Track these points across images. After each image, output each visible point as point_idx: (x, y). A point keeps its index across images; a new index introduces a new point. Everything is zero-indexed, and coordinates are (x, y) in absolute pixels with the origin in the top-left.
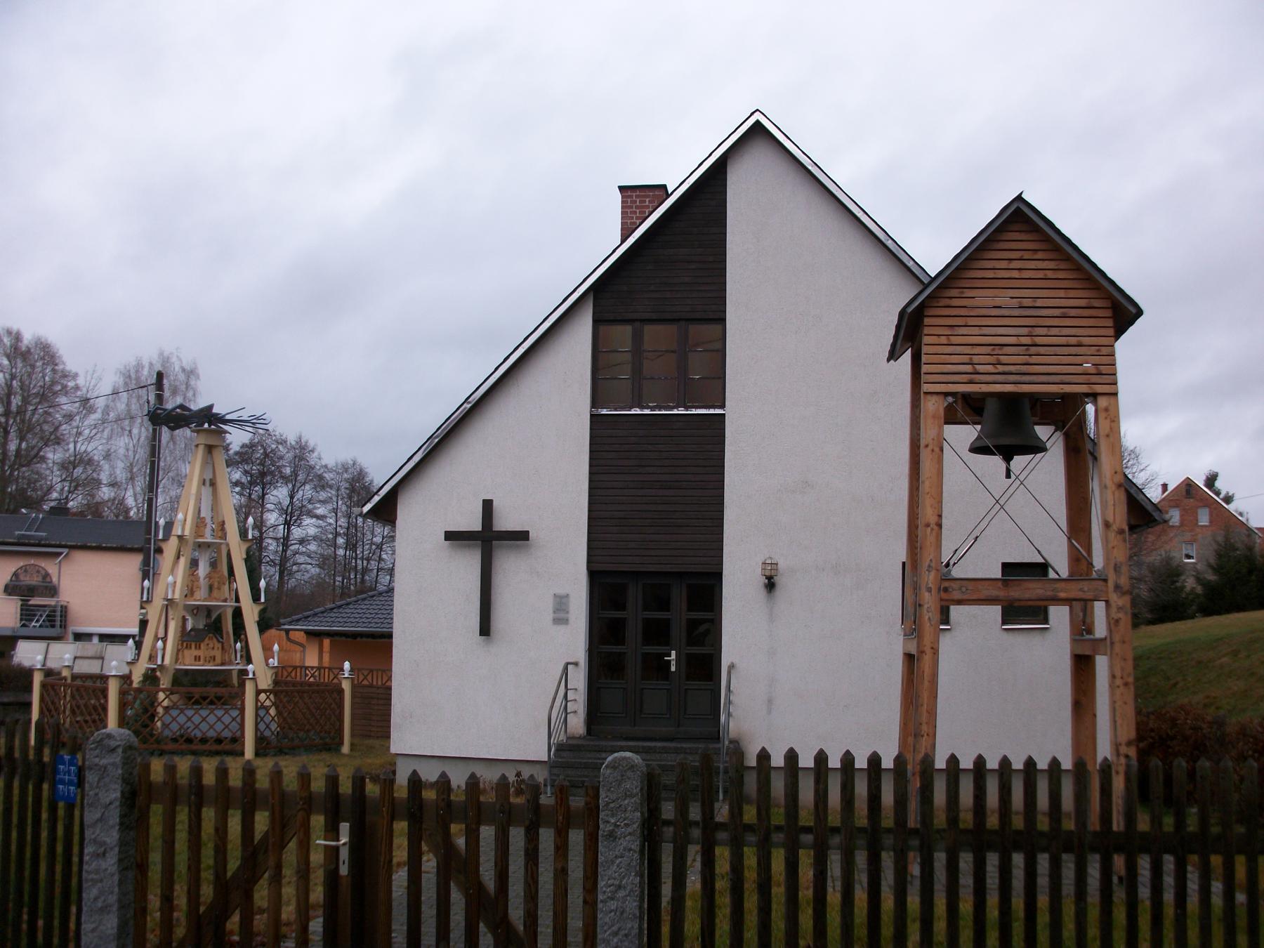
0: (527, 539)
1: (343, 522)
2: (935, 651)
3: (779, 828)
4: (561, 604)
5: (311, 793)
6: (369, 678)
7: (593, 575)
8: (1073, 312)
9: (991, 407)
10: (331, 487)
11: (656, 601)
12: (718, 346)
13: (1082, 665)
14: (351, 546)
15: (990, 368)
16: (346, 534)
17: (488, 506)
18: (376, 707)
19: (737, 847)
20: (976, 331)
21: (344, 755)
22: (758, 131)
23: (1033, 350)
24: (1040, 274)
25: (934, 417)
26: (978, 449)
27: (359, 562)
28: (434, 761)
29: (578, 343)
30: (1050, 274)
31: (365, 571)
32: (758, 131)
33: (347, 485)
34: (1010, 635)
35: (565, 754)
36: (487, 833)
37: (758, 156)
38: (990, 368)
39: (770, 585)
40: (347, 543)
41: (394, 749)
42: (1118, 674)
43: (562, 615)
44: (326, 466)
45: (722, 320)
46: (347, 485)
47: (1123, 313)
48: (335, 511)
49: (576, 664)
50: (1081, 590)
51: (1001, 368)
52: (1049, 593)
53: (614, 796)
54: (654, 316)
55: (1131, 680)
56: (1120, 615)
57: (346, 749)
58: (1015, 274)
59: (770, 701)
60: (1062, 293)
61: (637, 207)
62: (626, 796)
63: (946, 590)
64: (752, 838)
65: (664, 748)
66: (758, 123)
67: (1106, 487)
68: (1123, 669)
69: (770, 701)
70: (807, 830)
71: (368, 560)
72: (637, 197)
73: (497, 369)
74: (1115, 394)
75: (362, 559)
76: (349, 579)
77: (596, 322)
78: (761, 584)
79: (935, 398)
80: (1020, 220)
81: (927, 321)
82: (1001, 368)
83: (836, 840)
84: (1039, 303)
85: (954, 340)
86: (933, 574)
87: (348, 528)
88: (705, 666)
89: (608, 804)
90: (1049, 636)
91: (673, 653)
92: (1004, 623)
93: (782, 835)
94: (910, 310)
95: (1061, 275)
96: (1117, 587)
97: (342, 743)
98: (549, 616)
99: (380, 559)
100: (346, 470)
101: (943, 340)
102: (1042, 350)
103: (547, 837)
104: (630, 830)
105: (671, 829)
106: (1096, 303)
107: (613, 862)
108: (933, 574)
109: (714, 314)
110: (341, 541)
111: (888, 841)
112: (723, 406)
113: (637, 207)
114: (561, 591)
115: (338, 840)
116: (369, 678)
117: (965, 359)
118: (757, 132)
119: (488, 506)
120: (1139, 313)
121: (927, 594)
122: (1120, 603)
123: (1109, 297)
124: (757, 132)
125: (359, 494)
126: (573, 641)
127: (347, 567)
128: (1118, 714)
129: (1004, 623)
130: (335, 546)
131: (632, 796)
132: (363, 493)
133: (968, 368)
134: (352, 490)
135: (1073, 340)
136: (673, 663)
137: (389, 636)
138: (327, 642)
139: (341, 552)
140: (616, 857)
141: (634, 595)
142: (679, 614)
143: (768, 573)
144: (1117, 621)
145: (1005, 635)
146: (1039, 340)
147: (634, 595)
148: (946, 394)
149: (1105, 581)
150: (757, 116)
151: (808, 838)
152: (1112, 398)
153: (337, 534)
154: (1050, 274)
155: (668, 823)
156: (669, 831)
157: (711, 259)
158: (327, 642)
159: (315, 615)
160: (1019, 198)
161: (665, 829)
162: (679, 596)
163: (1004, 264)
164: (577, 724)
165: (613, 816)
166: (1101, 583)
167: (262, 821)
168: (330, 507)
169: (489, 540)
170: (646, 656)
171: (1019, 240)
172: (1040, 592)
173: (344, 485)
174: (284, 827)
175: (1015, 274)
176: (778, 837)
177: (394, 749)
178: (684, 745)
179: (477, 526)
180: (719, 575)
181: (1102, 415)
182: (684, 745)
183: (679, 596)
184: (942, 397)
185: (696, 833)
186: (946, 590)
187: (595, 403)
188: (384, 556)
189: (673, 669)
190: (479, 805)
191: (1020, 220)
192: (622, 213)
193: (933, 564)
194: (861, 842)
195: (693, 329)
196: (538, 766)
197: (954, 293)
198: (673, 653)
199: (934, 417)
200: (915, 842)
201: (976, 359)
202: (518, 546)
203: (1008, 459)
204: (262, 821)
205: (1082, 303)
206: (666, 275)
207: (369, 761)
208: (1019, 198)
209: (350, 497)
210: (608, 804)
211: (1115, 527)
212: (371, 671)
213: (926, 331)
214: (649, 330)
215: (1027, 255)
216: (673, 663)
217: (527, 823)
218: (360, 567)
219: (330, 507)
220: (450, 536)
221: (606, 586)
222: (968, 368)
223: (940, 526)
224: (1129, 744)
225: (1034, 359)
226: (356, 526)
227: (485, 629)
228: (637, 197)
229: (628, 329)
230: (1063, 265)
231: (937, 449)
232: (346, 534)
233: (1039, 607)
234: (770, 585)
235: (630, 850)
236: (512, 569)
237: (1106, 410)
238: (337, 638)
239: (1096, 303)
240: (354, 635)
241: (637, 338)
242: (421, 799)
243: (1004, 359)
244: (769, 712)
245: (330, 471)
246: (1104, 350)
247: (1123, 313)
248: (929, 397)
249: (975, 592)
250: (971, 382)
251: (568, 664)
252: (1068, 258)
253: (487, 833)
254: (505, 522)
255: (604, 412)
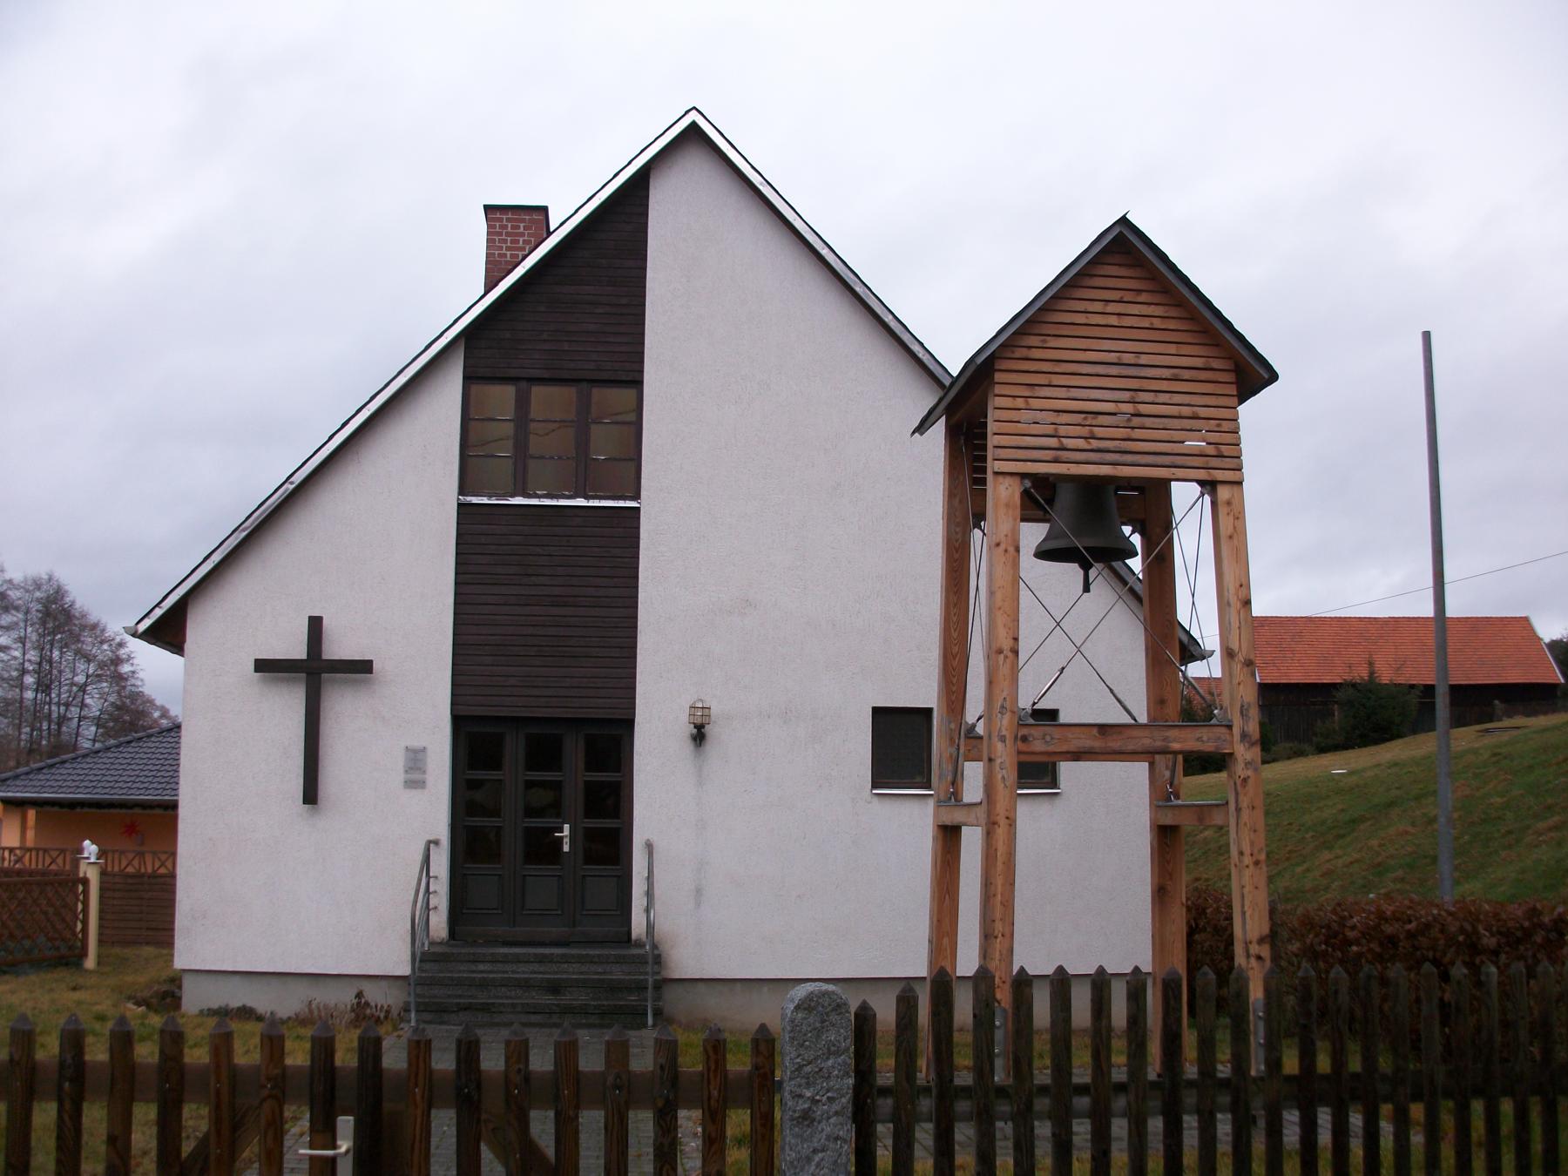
0: (370, 671)
1: (33, 655)
2: (1011, 822)
3: (1043, 1090)
4: (415, 760)
5: (285, 1068)
6: (60, 861)
7: (458, 721)
8: (1186, 374)
9: (1065, 497)
10: (17, 609)
11: (544, 757)
12: (632, 417)
13: (949, 835)
14: (44, 686)
15: (1081, 443)
16: (38, 672)
17: (315, 624)
18: (146, 906)
19: (984, 1120)
20: (1062, 393)
21: (91, 972)
22: (693, 138)
23: (1136, 421)
24: (1146, 323)
25: (1007, 505)
26: (1044, 554)
27: (54, 708)
28: (236, 979)
29: (445, 402)
30: (1157, 323)
31: (62, 720)
32: (693, 138)
33: (39, 607)
34: (887, 802)
35: (427, 966)
36: (592, 1121)
37: (693, 166)
38: (1081, 443)
39: (699, 736)
40: (38, 683)
41: (181, 962)
42: (1247, 851)
43: (416, 776)
44: (10, 581)
45: (638, 383)
46: (39, 607)
47: (1250, 373)
48: (22, 641)
49: (436, 843)
50: (1199, 739)
51: (1095, 444)
52: (1158, 744)
53: (809, 1055)
54: (546, 375)
55: (1263, 857)
56: (1249, 773)
57: (90, 963)
58: (1113, 320)
59: (699, 892)
60: (1172, 349)
61: (508, 234)
62: (830, 1053)
63: (1024, 739)
64: (1004, 1107)
65: (564, 955)
66: (694, 126)
67: (1229, 604)
68: (1252, 844)
69: (699, 892)
70: (1082, 1090)
71: (67, 705)
72: (511, 223)
73: (331, 438)
74: (1240, 483)
75: (59, 704)
76: (40, 729)
77: (468, 379)
78: (687, 734)
79: (1008, 481)
80: (1124, 252)
81: (998, 377)
82: (1095, 444)
83: (1120, 1103)
84: (1144, 360)
85: (1034, 403)
86: (1007, 716)
87: (40, 664)
88: (610, 843)
89: (800, 1067)
90: (1058, 802)
91: (566, 827)
92: (874, 786)
93: (1047, 1101)
94: (980, 360)
95: (1172, 325)
96: (1244, 736)
97: (85, 955)
98: (399, 776)
99: (83, 705)
100: (38, 587)
101: (1020, 403)
102: (1148, 422)
103: (689, 1122)
104: (836, 1107)
105: (890, 1101)
106: (1215, 364)
107: (809, 1160)
108: (1007, 716)
109: (628, 374)
110: (29, 680)
111: (1190, 1099)
112: (637, 497)
113: (508, 234)
114: (416, 743)
115: (334, 1147)
116: (60, 861)
117: (1049, 429)
118: (693, 138)
119: (315, 624)
120: (1273, 377)
121: (1000, 745)
122: (1249, 756)
123: (1232, 356)
124: (693, 138)
125: (55, 619)
126: (431, 813)
127: (37, 714)
128: (1247, 903)
129: (874, 786)
130: (22, 687)
131: (838, 1053)
132: (62, 618)
133: (1053, 442)
134: (47, 614)
135: (1186, 411)
136: (566, 840)
137: (173, 806)
138: (31, 814)
139: (29, 695)
140: (815, 1151)
141: (514, 749)
142: (575, 773)
143: (699, 721)
144: (1245, 780)
145: (876, 799)
146: (1143, 409)
147: (514, 749)
148: (1023, 476)
149: (1230, 727)
150: (694, 116)
151: (1082, 1102)
152: (1235, 488)
153: (24, 672)
154: (1157, 323)
155: (885, 1092)
156: (886, 1105)
157: (624, 301)
158: (31, 814)
159: (17, 777)
160: (1124, 221)
161: (880, 1101)
162: (574, 752)
163: (1098, 307)
164: (439, 924)
165: (808, 1085)
166: (1223, 730)
167: (196, 1119)
168: (15, 634)
169: (316, 672)
170: (528, 832)
171: (1116, 275)
172: (1147, 742)
173: (35, 607)
174: (235, 1128)
175: (1113, 320)
176: (1042, 1104)
177: (181, 962)
178: (592, 952)
179: (299, 652)
180: (629, 724)
181: (1222, 510)
182: (592, 952)
183: (574, 752)
184: (1017, 480)
185: (926, 1104)
186: (1024, 739)
187: (462, 490)
188: (88, 701)
189: (566, 848)
190: (577, 1077)
191: (1124, 252)
192: (488, 241)
193: (1007, 705)
194: (1155, 1103)
195: (598, 393)
196: (384, 983)
197: (1034, 341)
198: (566, 827)
199: (1007, 505)
200: (1225, 1099)
201: (1063, 430)
202: (356, 681)
203: (1086, 567)
204: (196, 1119)
205: (1198, 362)
206: (562, 322)
207: (129, 979)
208: (1124, 221)
209: (43, 623)
210: (800, 1067)
211: (1241, 657)
212: (63, 851)
213: (998, 389)
214: (538, 392)
215: (1128, 296)
216: (566, 840)
217: (660, 1104)
218: (55, 715)
219: (15, 634)
220: (262, 666)
221: (476, 740)
222: (1053, 442)
223: (1016, 652)
224: (1261, 941)
225: (1137, 434)
226: (50, 662)
227: (311, 795)
228: (511, 223)
229: (509, 391)
230: (1173, 312)
231: (1011, 549)
232: (38, 672)
233: (1045, 764)
234: (699, 736)
235: (837, 1138)
236: (346, 712)
237: (1229, 503)
238: (48, 808)
239: (1215, 364)
240: (73, 805)
241: (522, 403)
242: (479, 1070)
243: (1098, 431)
244: (698, 904)
245: (17, 587)
246: (1226, 426)
247: (1250, 373)
248: (1001, 478)
249: (1105, 743)
250: (1056, 461)
251: (430, 842)
252: (1180, 303)
253: (592, 1121)
254: (338, 647)
255: (475, 500)
